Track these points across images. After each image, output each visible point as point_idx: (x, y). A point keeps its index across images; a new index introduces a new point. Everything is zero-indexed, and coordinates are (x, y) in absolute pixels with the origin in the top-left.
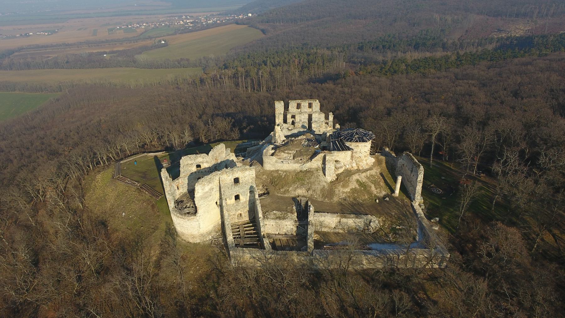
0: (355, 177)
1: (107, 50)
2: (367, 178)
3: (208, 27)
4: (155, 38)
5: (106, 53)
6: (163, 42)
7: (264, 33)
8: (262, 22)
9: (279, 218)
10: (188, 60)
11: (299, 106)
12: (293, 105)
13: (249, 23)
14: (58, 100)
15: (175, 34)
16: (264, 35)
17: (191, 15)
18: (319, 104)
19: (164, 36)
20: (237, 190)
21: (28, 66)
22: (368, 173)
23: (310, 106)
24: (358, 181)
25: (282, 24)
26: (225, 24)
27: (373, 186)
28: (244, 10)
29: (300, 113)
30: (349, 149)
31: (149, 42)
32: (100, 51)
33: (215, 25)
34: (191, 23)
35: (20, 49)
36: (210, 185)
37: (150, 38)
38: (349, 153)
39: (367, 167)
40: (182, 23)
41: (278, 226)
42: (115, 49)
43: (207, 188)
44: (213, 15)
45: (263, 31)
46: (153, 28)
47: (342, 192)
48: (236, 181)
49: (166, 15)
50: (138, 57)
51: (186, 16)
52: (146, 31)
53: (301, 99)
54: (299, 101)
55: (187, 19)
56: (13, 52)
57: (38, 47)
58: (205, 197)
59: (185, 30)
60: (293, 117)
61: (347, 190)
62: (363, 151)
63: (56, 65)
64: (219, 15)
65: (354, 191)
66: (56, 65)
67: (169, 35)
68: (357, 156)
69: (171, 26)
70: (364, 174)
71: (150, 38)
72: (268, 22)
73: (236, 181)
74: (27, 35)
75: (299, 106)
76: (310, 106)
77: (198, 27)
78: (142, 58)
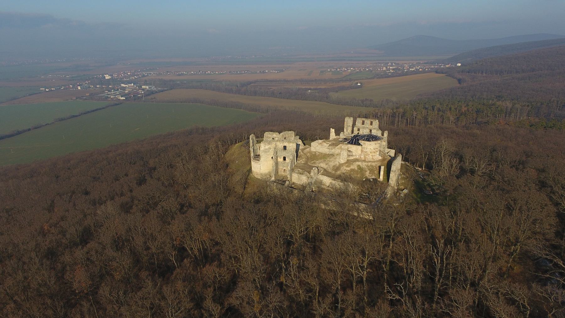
0: (358, 163)
1: (312, 87)
2: (367, 166)
3: (409, 73)
4: (354, 80)
5: (310, 89)
6: (359, 84)
7: (460, 83)
8: (462, 72)
9: (300, 173)
10: (371, 100)
11: (363, 123)
12: (359, 121)
13: (449, 73)
14: (262, 118)
15: (373, 78)
16: (459, 85)
17: (397, 62)
18: (378, 123)
19: (363, 79)
20: (284, 154)
21: (255, 93)
22: (370, 164)
23: (371, 123)
24: (359, 166)
25: (484, 75)
26: (428, 72)
27: (368, 171)
28: (455, 60)
29: (364, 128)
30: (359, 144)
31: (348, 84)
32: (307, 87)
33: (417, 72)
34: (393, 69)
35: (256, 82)
36: (269, 146)
37: (351, 80)
38: (360, 147)
39: (371, 160)
40: (384, 69)
41: (299, 179)
42: (319, 87)
43: (267, 147)
44: (419, 63)
45: (460, 81)
46: (358, 72)
47: (345, 169)
48: (285, 148)
49: (374, 62)
50: (331, 94)
51: (392, 63)
52: (350, 74)
53: (366, 117)
54: (364, 119)
55: (392, 66)
56: (251, 83)
57: (267, 81)
58: (266, 151)
59: (385, 75)
60: (359, 130)
61: (348, 169)
62: (369, 147)
63: (273, 95)
64: (425, 63)
65: (352, 170)
66: (273, 95)
67: (367, 79)
68: (365, 150)
69: (373, 72)
70: (366, 163)
71: (351, 80)
72: (469, 72)
73: (285, 148)
74: (264, 72)
75: (363, 123)
76: (371, 123)
77: (399, 73)
78: (334, 96)
